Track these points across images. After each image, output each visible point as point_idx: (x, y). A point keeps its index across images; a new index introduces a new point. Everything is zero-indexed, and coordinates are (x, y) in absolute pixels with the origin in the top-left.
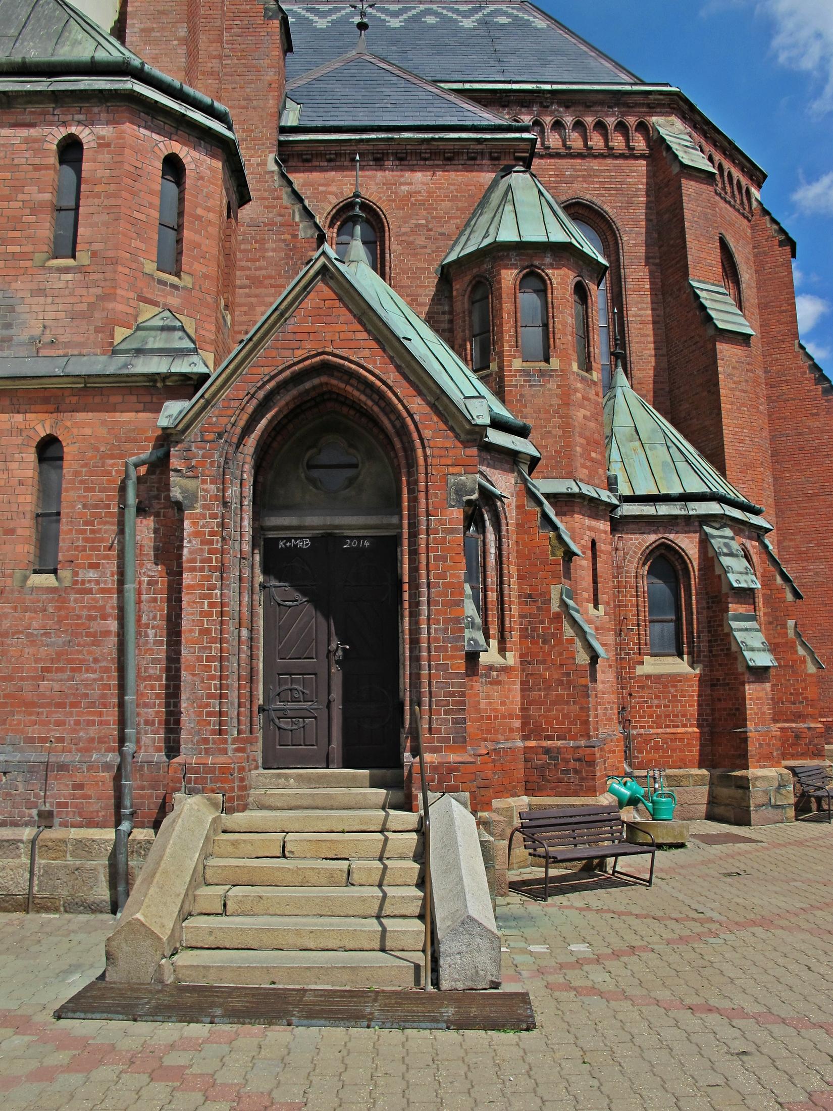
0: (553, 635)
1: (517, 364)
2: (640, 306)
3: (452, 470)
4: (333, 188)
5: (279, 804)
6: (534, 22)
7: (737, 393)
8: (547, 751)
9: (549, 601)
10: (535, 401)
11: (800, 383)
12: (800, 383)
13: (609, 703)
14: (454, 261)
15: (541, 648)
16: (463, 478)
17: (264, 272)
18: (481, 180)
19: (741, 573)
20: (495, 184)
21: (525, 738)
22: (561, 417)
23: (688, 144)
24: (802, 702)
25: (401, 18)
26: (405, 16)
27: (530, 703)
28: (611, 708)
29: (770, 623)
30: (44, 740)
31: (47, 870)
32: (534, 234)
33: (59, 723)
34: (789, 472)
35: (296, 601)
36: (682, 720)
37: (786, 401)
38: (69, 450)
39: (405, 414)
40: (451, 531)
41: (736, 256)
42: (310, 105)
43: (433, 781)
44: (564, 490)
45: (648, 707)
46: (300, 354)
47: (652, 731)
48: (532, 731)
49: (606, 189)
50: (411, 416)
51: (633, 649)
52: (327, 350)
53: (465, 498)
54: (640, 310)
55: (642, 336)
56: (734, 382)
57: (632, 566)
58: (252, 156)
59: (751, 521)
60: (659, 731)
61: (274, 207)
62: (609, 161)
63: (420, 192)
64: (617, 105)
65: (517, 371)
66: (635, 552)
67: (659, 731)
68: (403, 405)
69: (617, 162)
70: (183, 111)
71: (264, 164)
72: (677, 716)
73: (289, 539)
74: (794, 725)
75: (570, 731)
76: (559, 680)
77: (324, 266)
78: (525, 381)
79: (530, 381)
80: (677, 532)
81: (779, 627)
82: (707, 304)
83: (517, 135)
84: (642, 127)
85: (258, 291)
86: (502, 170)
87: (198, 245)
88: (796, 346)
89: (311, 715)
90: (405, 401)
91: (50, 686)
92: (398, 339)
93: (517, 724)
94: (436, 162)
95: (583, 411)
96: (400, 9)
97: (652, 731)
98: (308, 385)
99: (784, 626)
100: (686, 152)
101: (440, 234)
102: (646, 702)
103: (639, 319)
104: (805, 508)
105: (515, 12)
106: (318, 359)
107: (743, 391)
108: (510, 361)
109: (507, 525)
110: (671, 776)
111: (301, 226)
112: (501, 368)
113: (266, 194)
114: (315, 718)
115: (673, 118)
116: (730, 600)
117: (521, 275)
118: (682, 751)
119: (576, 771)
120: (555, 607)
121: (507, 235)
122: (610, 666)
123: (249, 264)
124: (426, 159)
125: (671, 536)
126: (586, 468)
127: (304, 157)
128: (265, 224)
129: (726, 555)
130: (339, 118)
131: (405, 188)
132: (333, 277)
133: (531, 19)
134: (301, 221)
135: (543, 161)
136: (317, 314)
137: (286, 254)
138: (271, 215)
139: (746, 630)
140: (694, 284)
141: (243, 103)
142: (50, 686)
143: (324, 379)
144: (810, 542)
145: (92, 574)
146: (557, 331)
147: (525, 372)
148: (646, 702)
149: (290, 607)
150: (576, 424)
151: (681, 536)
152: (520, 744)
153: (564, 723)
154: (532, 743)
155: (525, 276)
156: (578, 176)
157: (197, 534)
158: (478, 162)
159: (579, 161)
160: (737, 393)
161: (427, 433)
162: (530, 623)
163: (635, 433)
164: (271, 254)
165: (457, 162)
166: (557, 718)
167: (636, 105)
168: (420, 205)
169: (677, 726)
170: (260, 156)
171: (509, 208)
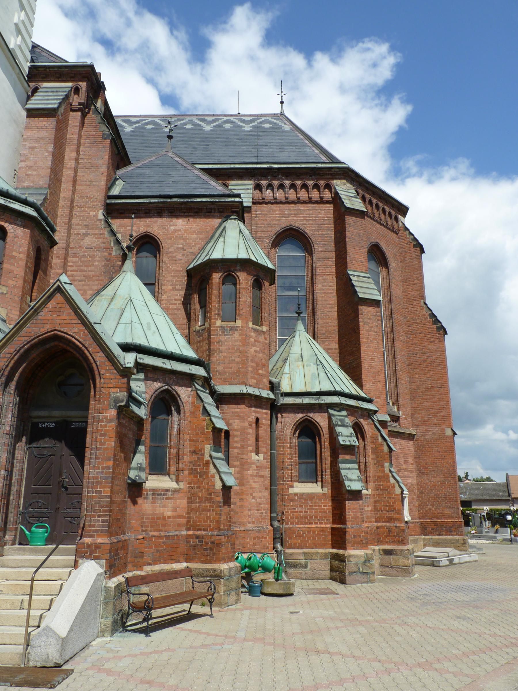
0: (205, 473)
1: (219, 323)
2: (323, 284)
3: (113, 390)
5: (13, 565)
6: (284, 127)
7: (370, 333)
8: (197, 537)
9: (203, 454)
10: (227, 343)
11: (424, 324)
12: (424, 324)
13: (264, 509)
14: (192, 268)
15: (198, 479)
16: (118, 394)
17: (93, 273)
18: (213, 223)
19: (347, 436)
20: (220, 224)
21: (189, 529)
22: (240, 352)
23: (352, 195)
24: (393, 511)
25: (212, 125)
26: (214, 124)
27: (192, 510)
28: (266, 513)
29: (375, 464)
32: (231, 253)
34: (418, 374)
35: (45, 455)
36: (315, 520)
37: (417, 334)
39: (92, 361)
40: (110, 421)
41: (387, 254)
42: (129, 182)
43: (87, 553)
44: (238, 391)
45: (296, 512)
46: (44, 330)
47: (297, 526)
48: (191, 526)
49: (307, 220)
50: (95, 362)
51: (287, 478)
52: (57, 328)
53: (118, 405)
54: (323, 286)
55: (323, 301)
56: (369, 327)
57: (288, 431)
58: (90, 211)
59: (362, 406)
60: (301, 526)
61: (100, 238)
62: (309, 205)
63: (180, 230)
64: (314, 175)
65: (218, 327)
66: (290, 424)
67: (301, 526)
68: (92, 357)
70: (6, 204)
71: (97, 215)
72: (312, 517)
73: (44, 423)
74: (388, 524)
75: (210, 526)
76: (206, 497)
77: (59, 286)
78: (222, 332)
79: (225, 332)
80: (314, 413)
81: (380, 467)
82: (355, 283)
83: (233, 199)
84: (328, 187)
85: (89, 283)
86: (225, 218)
88: (422, 303)
89: (46, 516)
90: (93, 355)
92: (90, 323)
93: (184, 521)
94: (190, 214)
95: (254, 348)
96: (213, 120)
97: (297, 526)
98: (48, 346)
99: (383, 466)
100: (349, 200)
101: (190, 253)
102: (294, 509)
103: (322, 291)
104: (427, 395)
105: (275, 121)
106: (52, 333)
107: (374, 331)
108: (215, 322)
109: (184, 413)
110: (306, 553)
111: (114, 249)
112: (210, 325)
113: (97, 232)
114: (48, 517)
115: (344, 181)
116: (340, 451)
117: (223, 276)
118: (314, 538)
119: (211, 549)
120: (207, 457)
121: (217, 255)
122: (266, 489)
123: (85, 268)
124: (184, 213)
125: (311, 415)
126: (255, 379)
127: (120, 211)
128: (95, 248)
129: (339, 426)
130: (142, 190)
131: (172, 228)
132: (63, 292)
133: (283, 125)
134: (114, 246)
135: (273, 206)
136: (54, 311)
137: (105, 264)
138: (98, 243)
139: (349, 469)
140: (349, 272)
141: (88, 183)
143: (56, 343)
144: (430, 415)
146: (241, 306)
147: (223, 328)
148: (294, 509)
149: (41, 458)
150: (249, 355)
151: (317, 414)
152: (184, 533)
153: (207, 522)
154: (191, 533)
155: (226, 277)
156: (292, 214)
158: (212, 214)
159: (292, 205)
161: (102, 371)
162: (194, 466)
163: (300, 357)
164: (97, 263)
165: (201, 214)
166: (204, 519)
167: (324, 174)
168: (180, 237)
169: (312, 524)
170: (95, 211)
171: (221, 239)
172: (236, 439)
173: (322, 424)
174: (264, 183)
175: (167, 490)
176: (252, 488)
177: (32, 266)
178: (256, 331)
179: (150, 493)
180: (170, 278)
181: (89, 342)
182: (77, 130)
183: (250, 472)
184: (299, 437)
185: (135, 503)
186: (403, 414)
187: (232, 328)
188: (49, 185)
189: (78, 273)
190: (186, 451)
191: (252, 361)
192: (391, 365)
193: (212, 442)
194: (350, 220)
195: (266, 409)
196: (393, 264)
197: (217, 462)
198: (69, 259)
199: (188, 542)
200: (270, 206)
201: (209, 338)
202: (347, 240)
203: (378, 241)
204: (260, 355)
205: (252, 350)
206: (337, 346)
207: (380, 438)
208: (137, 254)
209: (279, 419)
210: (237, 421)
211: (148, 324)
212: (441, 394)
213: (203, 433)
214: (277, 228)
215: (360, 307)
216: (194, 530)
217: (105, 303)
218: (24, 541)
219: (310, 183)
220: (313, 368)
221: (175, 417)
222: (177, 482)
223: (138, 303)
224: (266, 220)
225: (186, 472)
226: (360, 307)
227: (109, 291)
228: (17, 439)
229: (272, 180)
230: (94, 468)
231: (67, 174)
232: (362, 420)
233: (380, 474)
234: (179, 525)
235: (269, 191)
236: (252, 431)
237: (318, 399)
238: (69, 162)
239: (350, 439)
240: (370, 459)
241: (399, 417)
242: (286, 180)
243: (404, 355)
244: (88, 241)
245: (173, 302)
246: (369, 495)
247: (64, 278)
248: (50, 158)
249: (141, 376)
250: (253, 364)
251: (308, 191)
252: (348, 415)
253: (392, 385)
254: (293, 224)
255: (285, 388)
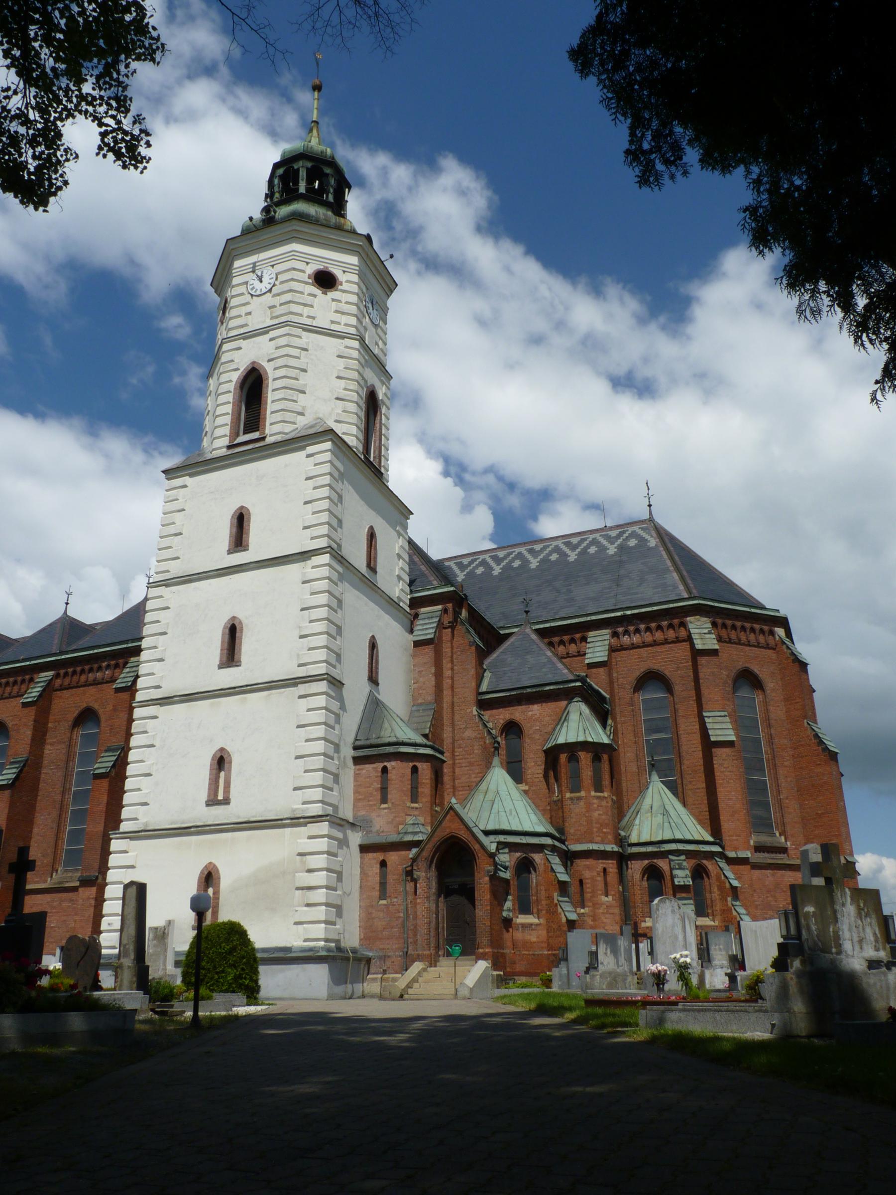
1: (568, 795)
4: (501, 717)
8: (554, 955)
9: (553, 899)
12: (809, 746)
21: (549, 950)
22: (586, 817)
27: (550, 937)
30: (384, 949)
31: (385, 986)
32: (572, 739)
33: (388, 944)
38: (388, 864)
41: (760, 676)
44: (586, 849)
46: (446, 833)
57: (637, 876)
62: (666, 646)
69: (670, 645)
71: (472, 712)
87: (423, 792)
88: (806, 723)
91: (385, 933)
93: (546, 945)
95: (598, 812)
99: (726, 901)
107: (731, 772)
120: (556, 901)
121: (561, 740)
125: (655, 861)
129: (677, 869)
131: (530, 713)
135: (631, 651)
142: (385, 933)
145: (395, 900)
147: (571, 799)
152: (546, 952)
154: (550, 952)
157: (421, 888)
159: (650, 648)
160: (726, 773)
161: (479, 855)
171: (565, 724)
172: (588, 886)
173: (664, 868)
174: (620, 630)
175: (531, 925)
176: (603, 923)
177: (434, 785)
178: (598, 798)
179: (520, 926)
180: (532, 755)
181: (470, 838)
182: (449, 645)
183: (601, 911)
184: (648, 880)
185: (508, 931)
186: (791, 845)
187: (579, 799)
188: (436, 700)
189: (464, 760)
190: (543, 898)
191: (596, 823)
192: (775, 794)
193: (558, 890)
194: (703, 661)
195: (612, 860)
196: (769, 684)
197: (563, 905)
198: (456, 750)
199: (549, 959)
200: (628, 651)
201: (562, 808)
202: (701, 681)
203: (747, 665)
204: (604, 817)
205: (596, 814)
206: (704, 785)
207: (723, 876)
208: (506, 737)
209: (630, 866)
210: (587, 872)
211: (511, 810)
212: (832, 820)
213: (552, 885)
214: (637, 673)
215: (714, 750)
216: (552, 951)
217: (481, 797)
218: (449, 954)
219: (665, 623)
220: (659, 819)
221: (533, 876)
222: (538, 919)
223: (503, 794)
224: (626, 667)
225: (544, 912)
226: (714, 750)
227: (483, 786)
228: (439, 896)
229: (627, 626)
230: (480, 910)
231: (447, 682)
232: (705, 862)
233: (725, 908)
234: (543, 948)
235: (626, 636)
236: (600, 879)
237: (659, 847)
238: (447, 673)
239: (685, 880)
240: (716, 895)
241: (787, 848)
242: (641, 624)
243: (791, 781)
244: (468, 733)
245: (537, 776)
246: (716, 926)
247: (454, 801)
248: (433, 679)
249: (507, 850)
250: (597, 825)
251: (663, 631)
252: (687, 858)
253: (778, 814)
254: (652, 666)
255: (634, 839)
